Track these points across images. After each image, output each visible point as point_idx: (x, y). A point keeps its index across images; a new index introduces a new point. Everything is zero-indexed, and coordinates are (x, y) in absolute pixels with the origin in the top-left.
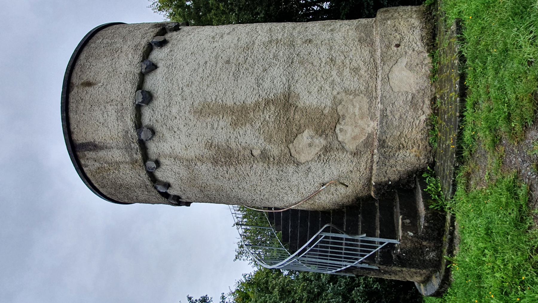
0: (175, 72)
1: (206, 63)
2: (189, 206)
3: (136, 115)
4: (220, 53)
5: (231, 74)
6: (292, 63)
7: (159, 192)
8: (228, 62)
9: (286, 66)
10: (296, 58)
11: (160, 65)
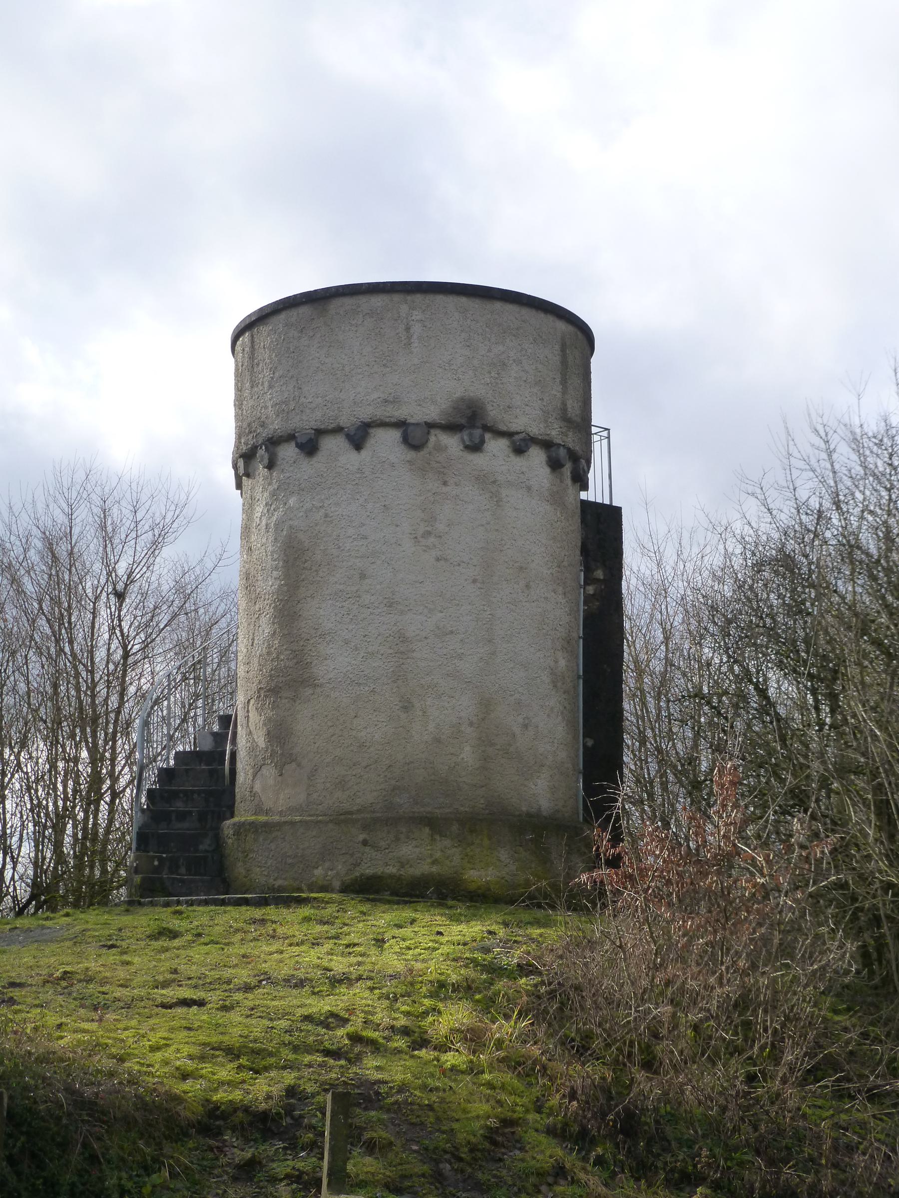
0: (350, 486)
1: (365, 538)
2: (620, 509)
3: (281, 437)
4: (384, 558)
5: (341, 587)
6: (359, 684)
7: (564, 404)
8: (363, 576)
9: (351, 676)
10: (367, 689)
11: (364, 453)
